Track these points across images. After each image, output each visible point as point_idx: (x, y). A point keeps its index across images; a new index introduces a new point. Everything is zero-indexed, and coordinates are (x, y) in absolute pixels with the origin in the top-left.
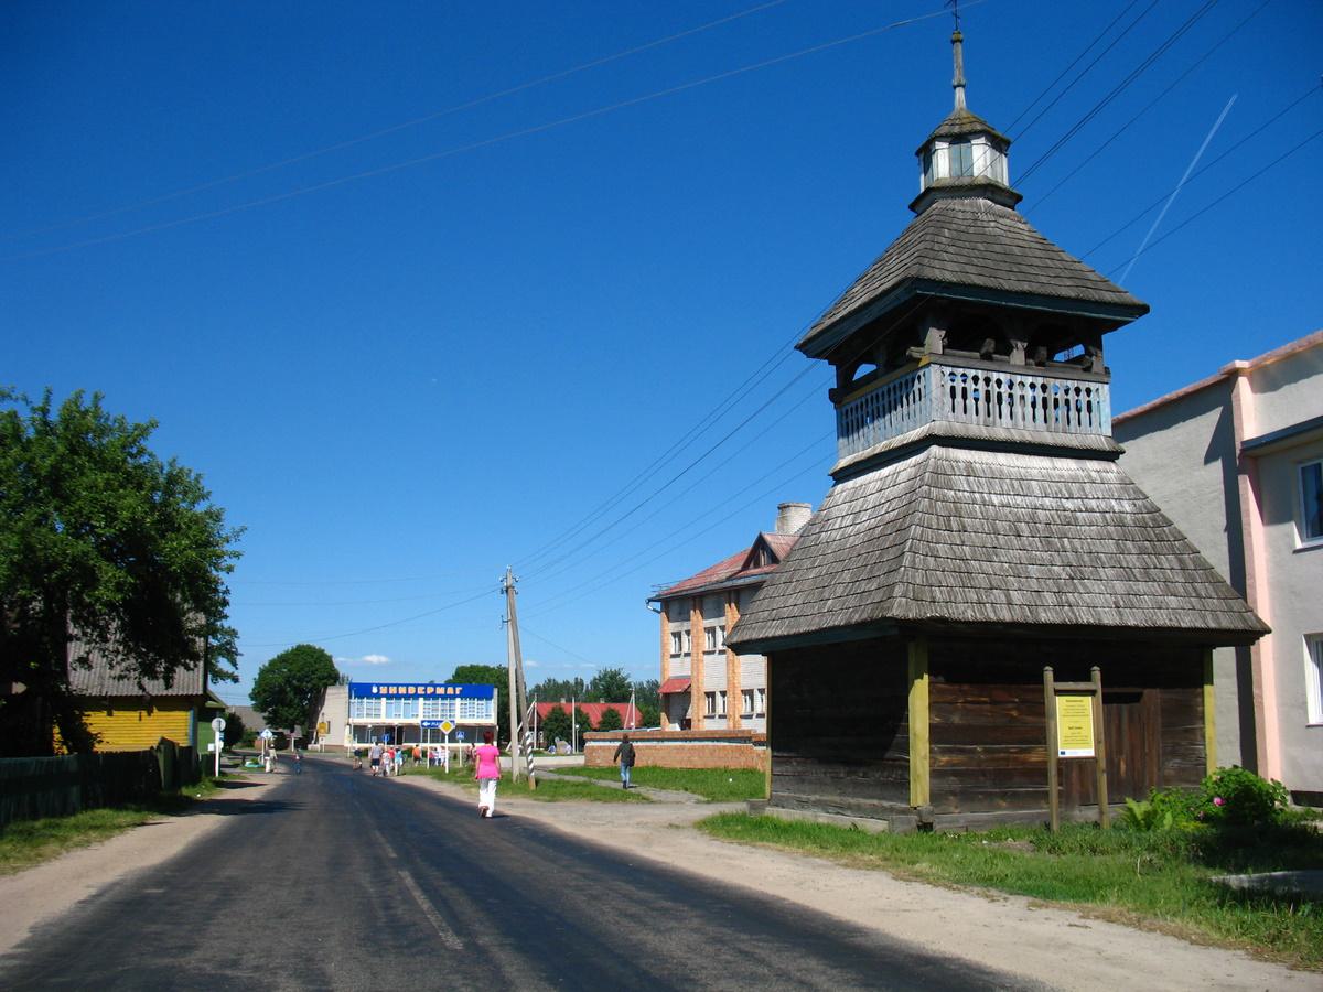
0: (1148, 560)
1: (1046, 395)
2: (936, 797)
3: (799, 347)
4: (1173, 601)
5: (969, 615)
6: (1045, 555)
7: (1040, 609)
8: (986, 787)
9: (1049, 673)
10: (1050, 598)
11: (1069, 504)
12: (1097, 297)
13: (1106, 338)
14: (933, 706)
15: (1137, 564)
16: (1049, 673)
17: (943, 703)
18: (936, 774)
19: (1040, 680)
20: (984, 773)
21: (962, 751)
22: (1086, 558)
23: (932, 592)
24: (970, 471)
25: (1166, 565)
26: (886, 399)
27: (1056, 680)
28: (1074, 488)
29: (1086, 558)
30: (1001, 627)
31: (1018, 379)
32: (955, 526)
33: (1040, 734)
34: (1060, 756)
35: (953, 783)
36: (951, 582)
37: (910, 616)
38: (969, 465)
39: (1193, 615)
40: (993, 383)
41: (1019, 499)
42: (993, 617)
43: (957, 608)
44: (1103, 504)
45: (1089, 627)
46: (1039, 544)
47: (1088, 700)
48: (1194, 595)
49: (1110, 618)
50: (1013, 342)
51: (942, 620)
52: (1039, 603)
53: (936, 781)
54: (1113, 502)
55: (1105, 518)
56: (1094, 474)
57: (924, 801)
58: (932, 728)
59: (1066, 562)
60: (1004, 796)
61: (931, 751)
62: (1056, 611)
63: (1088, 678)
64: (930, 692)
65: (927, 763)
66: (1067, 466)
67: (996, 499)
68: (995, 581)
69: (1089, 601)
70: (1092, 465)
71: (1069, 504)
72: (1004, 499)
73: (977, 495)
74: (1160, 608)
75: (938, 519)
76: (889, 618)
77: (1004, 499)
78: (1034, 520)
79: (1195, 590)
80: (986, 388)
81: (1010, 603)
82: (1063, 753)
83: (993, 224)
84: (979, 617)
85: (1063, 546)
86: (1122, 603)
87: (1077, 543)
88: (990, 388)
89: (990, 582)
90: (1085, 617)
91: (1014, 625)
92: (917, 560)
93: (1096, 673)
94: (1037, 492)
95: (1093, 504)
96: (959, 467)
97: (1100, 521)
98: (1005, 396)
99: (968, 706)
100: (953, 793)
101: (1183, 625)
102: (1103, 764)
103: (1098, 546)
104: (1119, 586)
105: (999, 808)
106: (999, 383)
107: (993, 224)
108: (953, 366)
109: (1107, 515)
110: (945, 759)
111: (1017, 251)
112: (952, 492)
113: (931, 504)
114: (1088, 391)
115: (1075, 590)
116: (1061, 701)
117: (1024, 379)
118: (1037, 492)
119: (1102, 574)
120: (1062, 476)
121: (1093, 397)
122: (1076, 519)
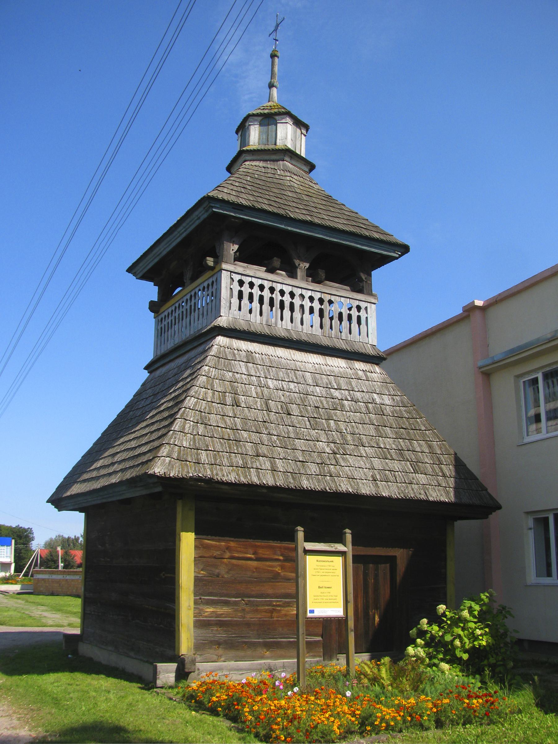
0: (402, 444)
1: (323, 307)
2: (199, 646)
3: (129, 270)
4: (422, 479)
5: (232, 478)
6: (313, 432)
7: (304, 477)
8: (249, 637)
9: (301, 535)
10: (313, 468)
11: (336, 394)
12: (368, 234)
13: (376, 274)
14: (198, 560)
15: (394, 446)
16: (301, 535)
17: (208, 557)
18: (201, 624)
19: (292, 538)
20: (248, 625)
21: (226, 603)
22: (349, 437)
23: (198, 454)
24: (250, 358)
25: (418, 449)
26: (189, 304)
27: (307, 539)
28: (342, 381)
29: (349, 437)
30: (264, 491)
31: (300, 288)
32: (229, 400)
33: (294, 590)
34: (309, 615)
35: (221, 634)
36: (218, 447)
37: (171, 475)
38: (249, 353)
39: (439, 490)
40: (277, 292)
41: (292, 385)
42: (256, 480)
43: (222, 470)
44: (367, 396)
45: (347, 495)
46: (308, 423)
47: (339, 560)
48: (440, 474)
49: (366, 489)
50: (297, 262)
51: (209, 481)
52: (302, 471)
53: (200, 631)
54: (375, 396)
55: (367, 407)
56: (360, 373)
57: (188, 648)
58: (198, 581)
59: (331, 440)
60: (268, 646)
61: (196, 603)
62: (318, 479)
63: (341, 540)
64: (196, 547)
65: (191, 613)
66: (338, 364)
67: (271, 383)
68: (263, 450)
69: (349, 473)
70: (359, 365)
71: (336, 394)
72: (279, 384)
73: (254, 378)
74: (411, 483)
75: (214, 394)
76: (151, 475)
77: (279, 384)
78: (303, 404)
79: (441, 469)
80: (270, 295)
81: (274, 470)
82: (312, 611)
83: (288, 178)
84: (243, 480)
85: (329, 426)
86: (378, 477)
87: (342, 426)
88: (274, 296)
89: (257, 450)
90: (345, 486)
91: (276, 489)
92: (187, 426)
93: (349, 537)
94: (310, 381)
95: (358, 395)
96: (240, 355)
97: (364, 410)
98: (287, 305)
99: (234, 561)
100: (219, 644)
101: (431, 499)
102: (351, 624)
103: (360, 429)
104: (377, 463)
105: (262, 658)
106: (282, 293)
107: (288, 178)
108: (242, 274)
109: (370, 405)
110: (210, 610)
111: (305, 198)
112: (230, 374)
113: (208, 381)
114: (359, 308)
115: (337, 463)
116: (311, 560)
117: (304, 292)
118: (310, 381)
119: (363, 452)
120: (333, 372)
121: (363, 314)
122: (343, 406)
